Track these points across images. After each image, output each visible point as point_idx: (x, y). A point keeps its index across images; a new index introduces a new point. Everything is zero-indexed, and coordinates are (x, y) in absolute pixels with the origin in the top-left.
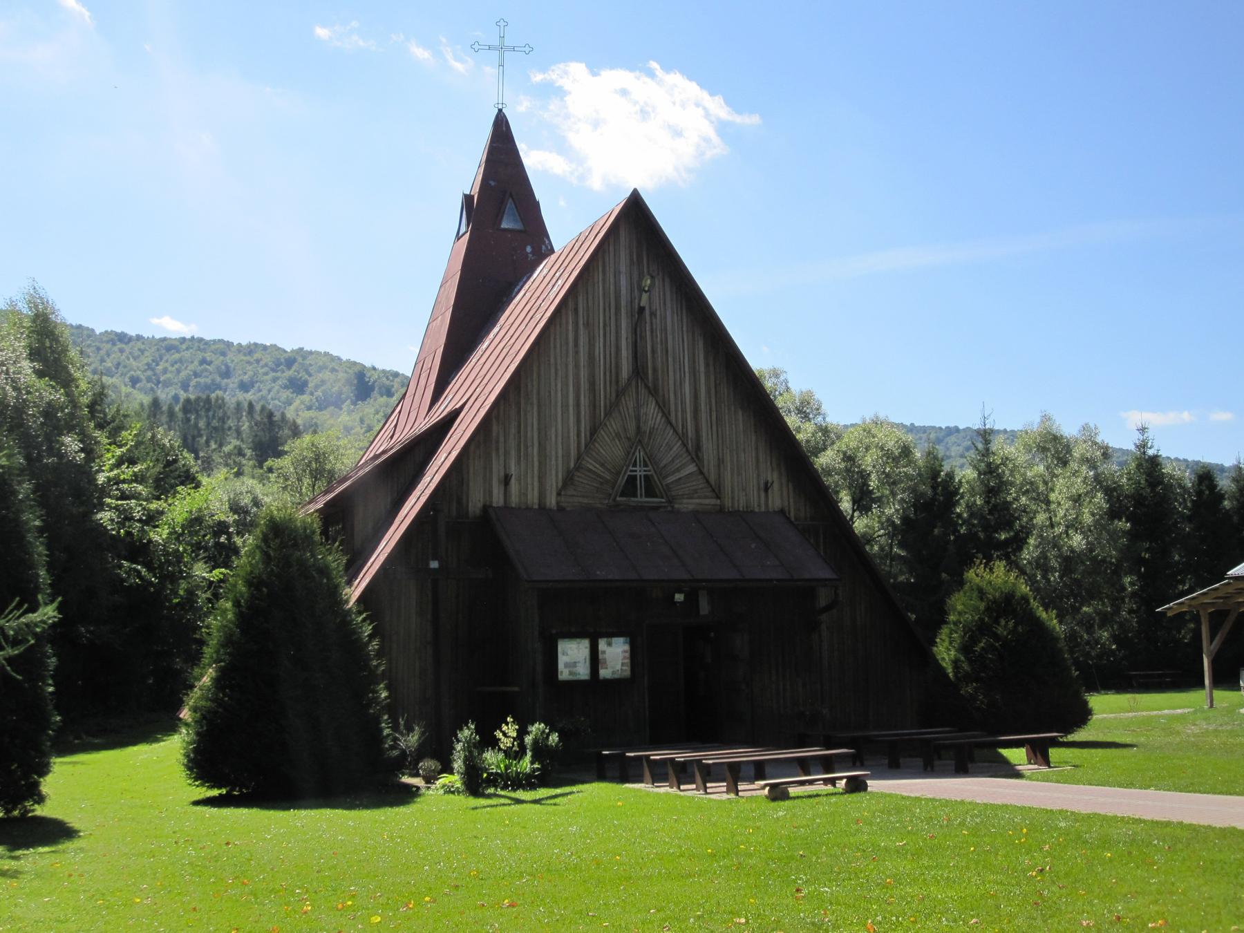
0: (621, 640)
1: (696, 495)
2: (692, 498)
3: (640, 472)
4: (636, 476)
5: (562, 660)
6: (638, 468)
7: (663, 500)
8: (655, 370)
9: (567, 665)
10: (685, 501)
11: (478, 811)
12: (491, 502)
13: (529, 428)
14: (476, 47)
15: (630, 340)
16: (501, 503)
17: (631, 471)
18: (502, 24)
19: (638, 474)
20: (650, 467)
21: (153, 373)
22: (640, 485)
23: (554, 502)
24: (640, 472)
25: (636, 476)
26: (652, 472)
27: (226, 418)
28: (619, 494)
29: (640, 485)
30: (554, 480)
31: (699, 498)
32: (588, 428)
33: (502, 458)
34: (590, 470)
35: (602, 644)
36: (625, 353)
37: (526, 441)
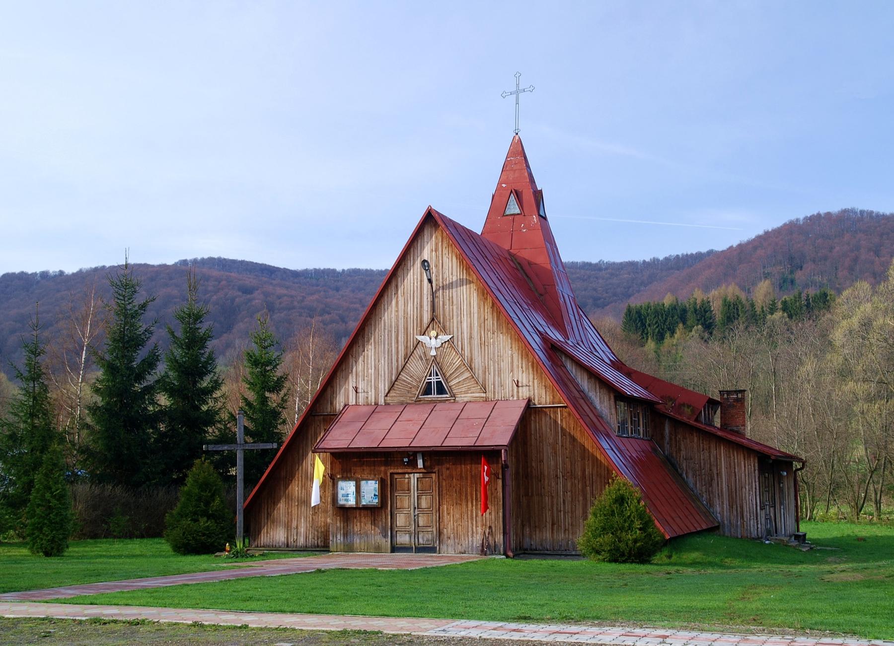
0: (373, 482)
1: (470, 392)
2: (468, 393)
3: (434, 379)
4: (431, 382)
5: (341, 493)
6: (432, 378)
7: (447, 396)
8: (444, 315)
9: (343, 496)
10: (463, 395)
11: (279, 608)
12: (348, 402)
13: (369, 359)
14: (517, 76)
15: (429, 299)
16: (354, 403)
17: (428, 379)
18: (518, 76)
19: (432, 381)
20: (440, 377)
21: (863, 484)
22: (434, 387)
23: (383, 401)
24: (434, 379)
25: (431, 382)
26: (441, 379)
27: (199, 321)
28: (420, 394)
29: (434, 387)
30: (383, 387)
31: (471, 393)
32: (403, 355)
33: (355, 377)
34: (404, 381)
35: (363, 483)
36: (427, 307)
37: (367, 367)
